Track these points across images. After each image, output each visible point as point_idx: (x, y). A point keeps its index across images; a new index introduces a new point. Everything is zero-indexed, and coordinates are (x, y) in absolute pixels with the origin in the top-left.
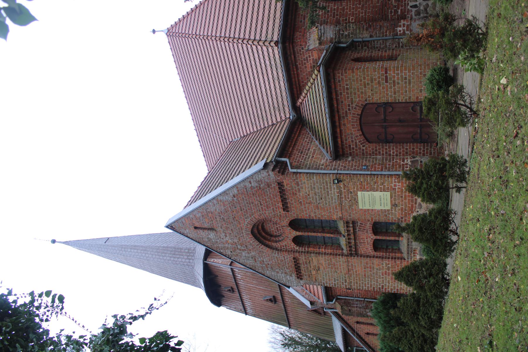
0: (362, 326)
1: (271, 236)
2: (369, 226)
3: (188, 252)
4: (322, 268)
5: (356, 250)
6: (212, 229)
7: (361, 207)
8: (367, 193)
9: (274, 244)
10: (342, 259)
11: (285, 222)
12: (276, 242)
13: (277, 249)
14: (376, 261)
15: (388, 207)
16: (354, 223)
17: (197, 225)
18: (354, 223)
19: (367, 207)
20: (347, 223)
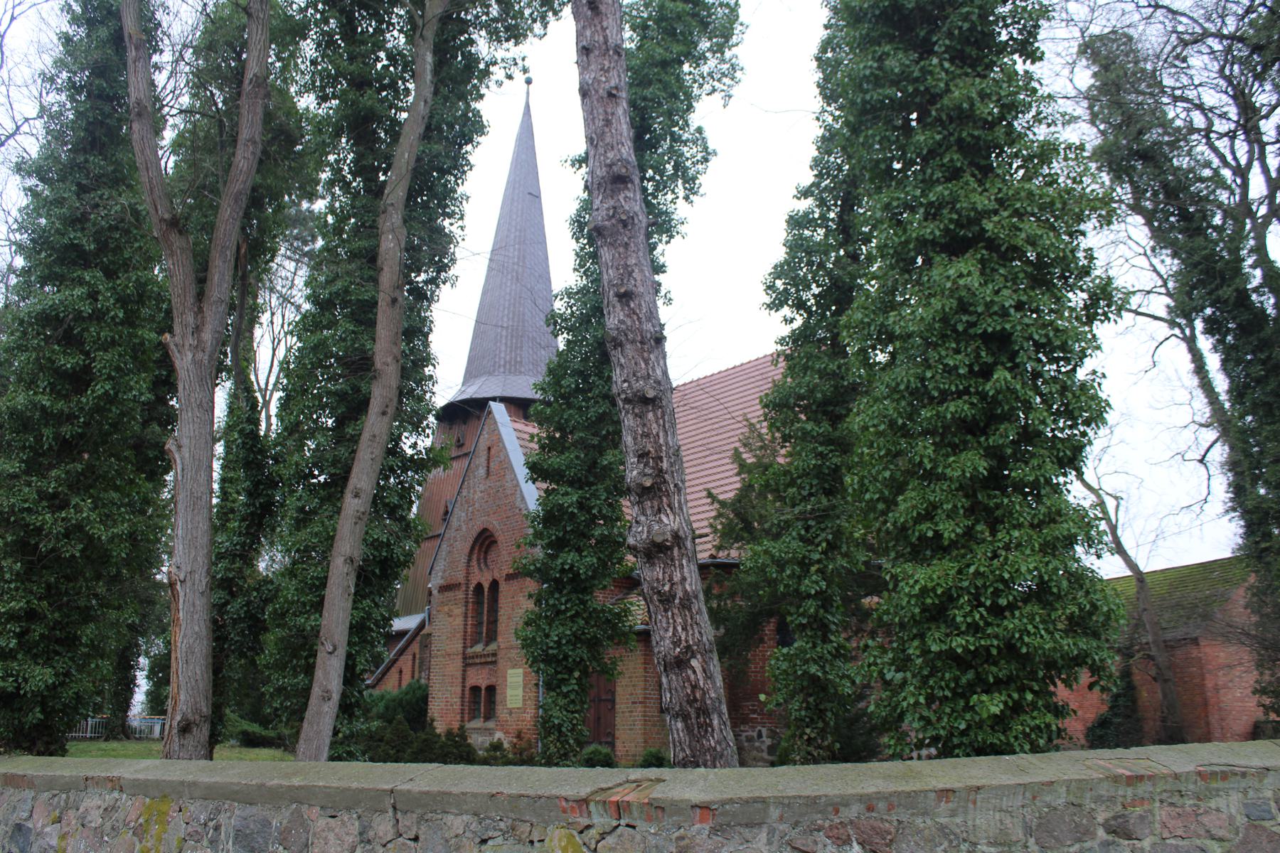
0: (410, 663)
1: (486, 553)
2: (492, 681)
3: (516, 362)
4: (451, 619)
5: (470, 665)
6: (488, 473)
7: (510, 671)
8: (521, 679)
9: (475, 557)
10: (460, 646)
11: (497, 576)
12: (478, 560)
13: (469, 560)
14: (459, 689)
15: (509, 706)
16: (494, 663)
17: (493, 451)
18: (494, 663)
19: (509, 680)
20: (494, 655)
